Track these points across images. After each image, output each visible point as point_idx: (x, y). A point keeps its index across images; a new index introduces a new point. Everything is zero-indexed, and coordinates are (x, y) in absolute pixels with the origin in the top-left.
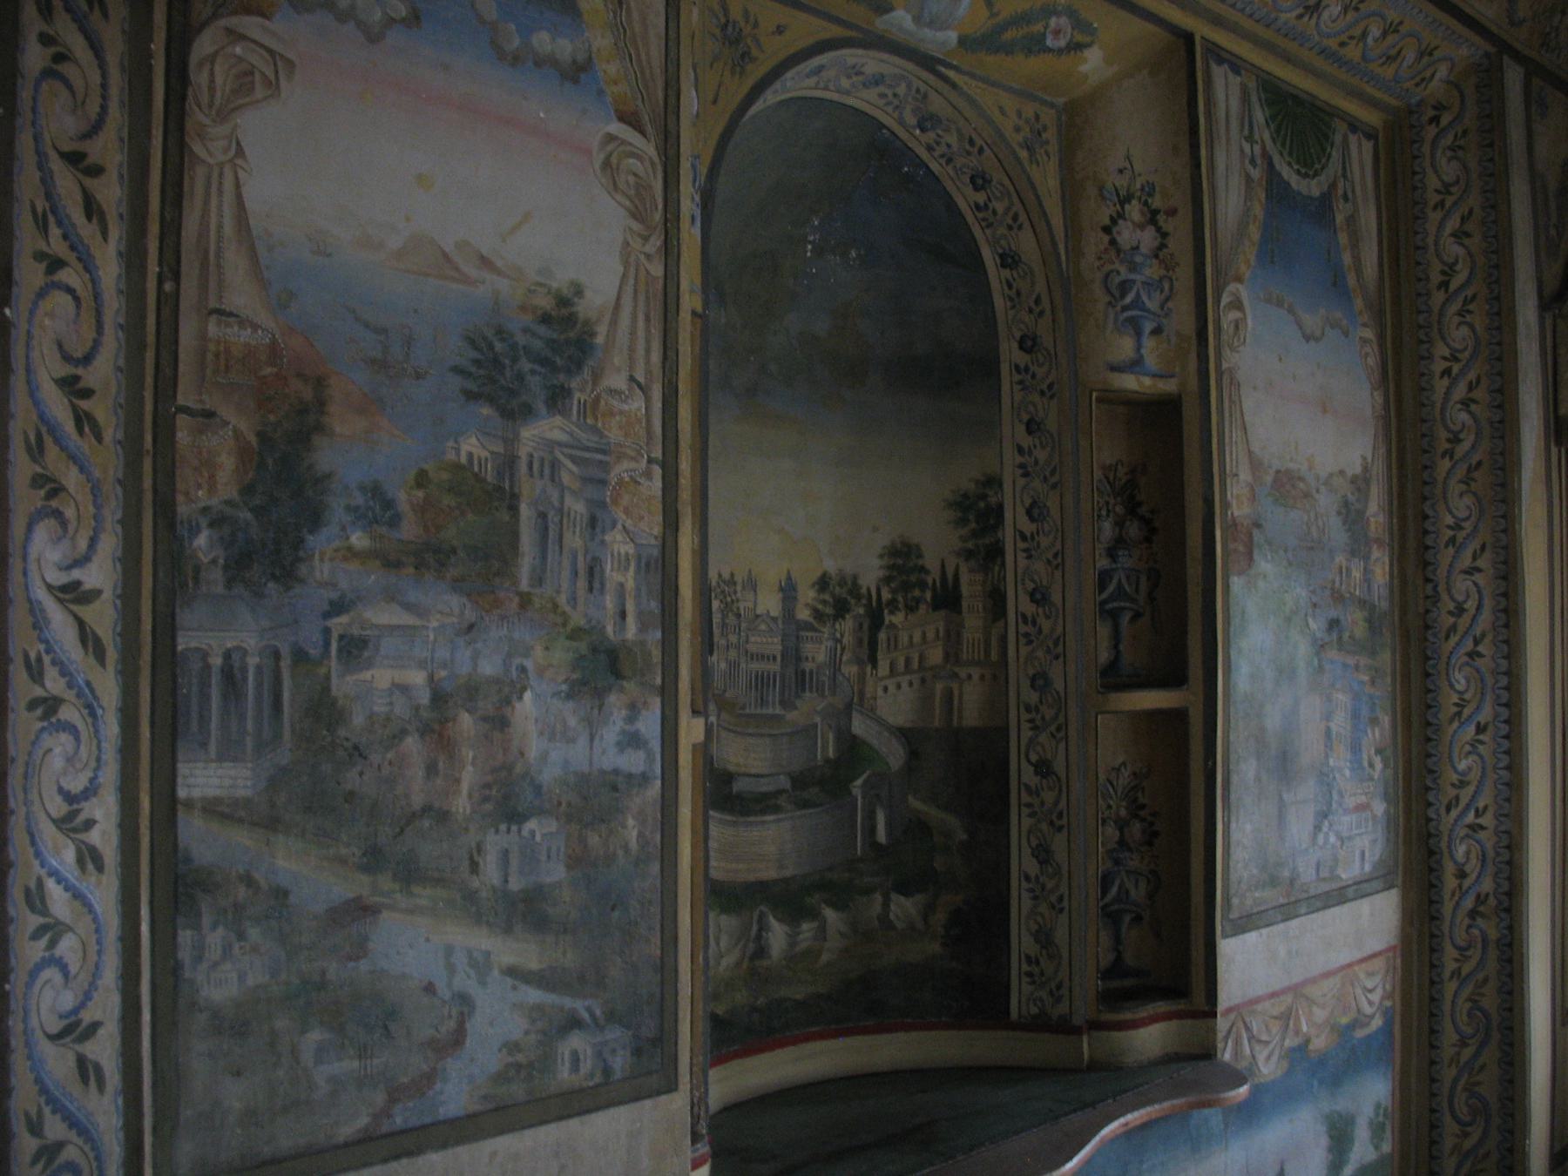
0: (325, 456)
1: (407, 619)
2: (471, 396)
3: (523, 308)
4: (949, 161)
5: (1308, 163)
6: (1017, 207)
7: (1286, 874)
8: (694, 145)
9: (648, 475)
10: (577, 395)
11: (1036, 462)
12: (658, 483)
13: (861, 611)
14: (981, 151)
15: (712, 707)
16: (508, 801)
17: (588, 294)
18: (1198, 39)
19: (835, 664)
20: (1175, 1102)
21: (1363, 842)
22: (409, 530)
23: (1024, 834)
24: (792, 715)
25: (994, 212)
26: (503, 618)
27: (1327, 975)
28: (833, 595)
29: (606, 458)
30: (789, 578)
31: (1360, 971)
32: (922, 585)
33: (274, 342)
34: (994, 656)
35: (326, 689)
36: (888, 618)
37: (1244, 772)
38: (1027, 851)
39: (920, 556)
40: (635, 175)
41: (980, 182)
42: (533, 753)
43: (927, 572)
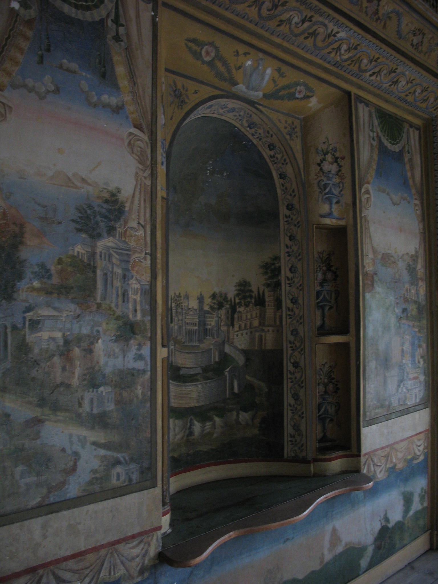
0: (24, 253)
1: (55, 313)
2: (79, 230)
3: (98, 198)
4: (260, 139)
5: (394, 138)
6: (285, 157)
7: (387, 403)
8: (162, 135)
9: (145, 258)
10: (118, 229)
11: (293, 251)
12: (149, 262)
13: (228, 306)
14: (272, 136)
15: (172, 343)
16: (93, 381)
17: (122, 192)
18: (352, 94)
19: (218, 326)
20: (346, 489)
21: (416, 391)
22: (55, 280)
23: (289, 389)
24: (202, 346)
25: (277, 158)
26: (91, 312)
27: (402, 441)
28: (217, 301)
29: (129, 253)
30: (201, 295)
31: (415, 439)
32: (251, 297)
33: (4, 210)
34: (278, 323)
35: (24, 340)
36: (238, 309)
37: (371, 366)
38: (290, 395)
39: (250, 286)
40: (140, 148)
41: (272, 147)
42: (102, 363)
43: (253, 292)
